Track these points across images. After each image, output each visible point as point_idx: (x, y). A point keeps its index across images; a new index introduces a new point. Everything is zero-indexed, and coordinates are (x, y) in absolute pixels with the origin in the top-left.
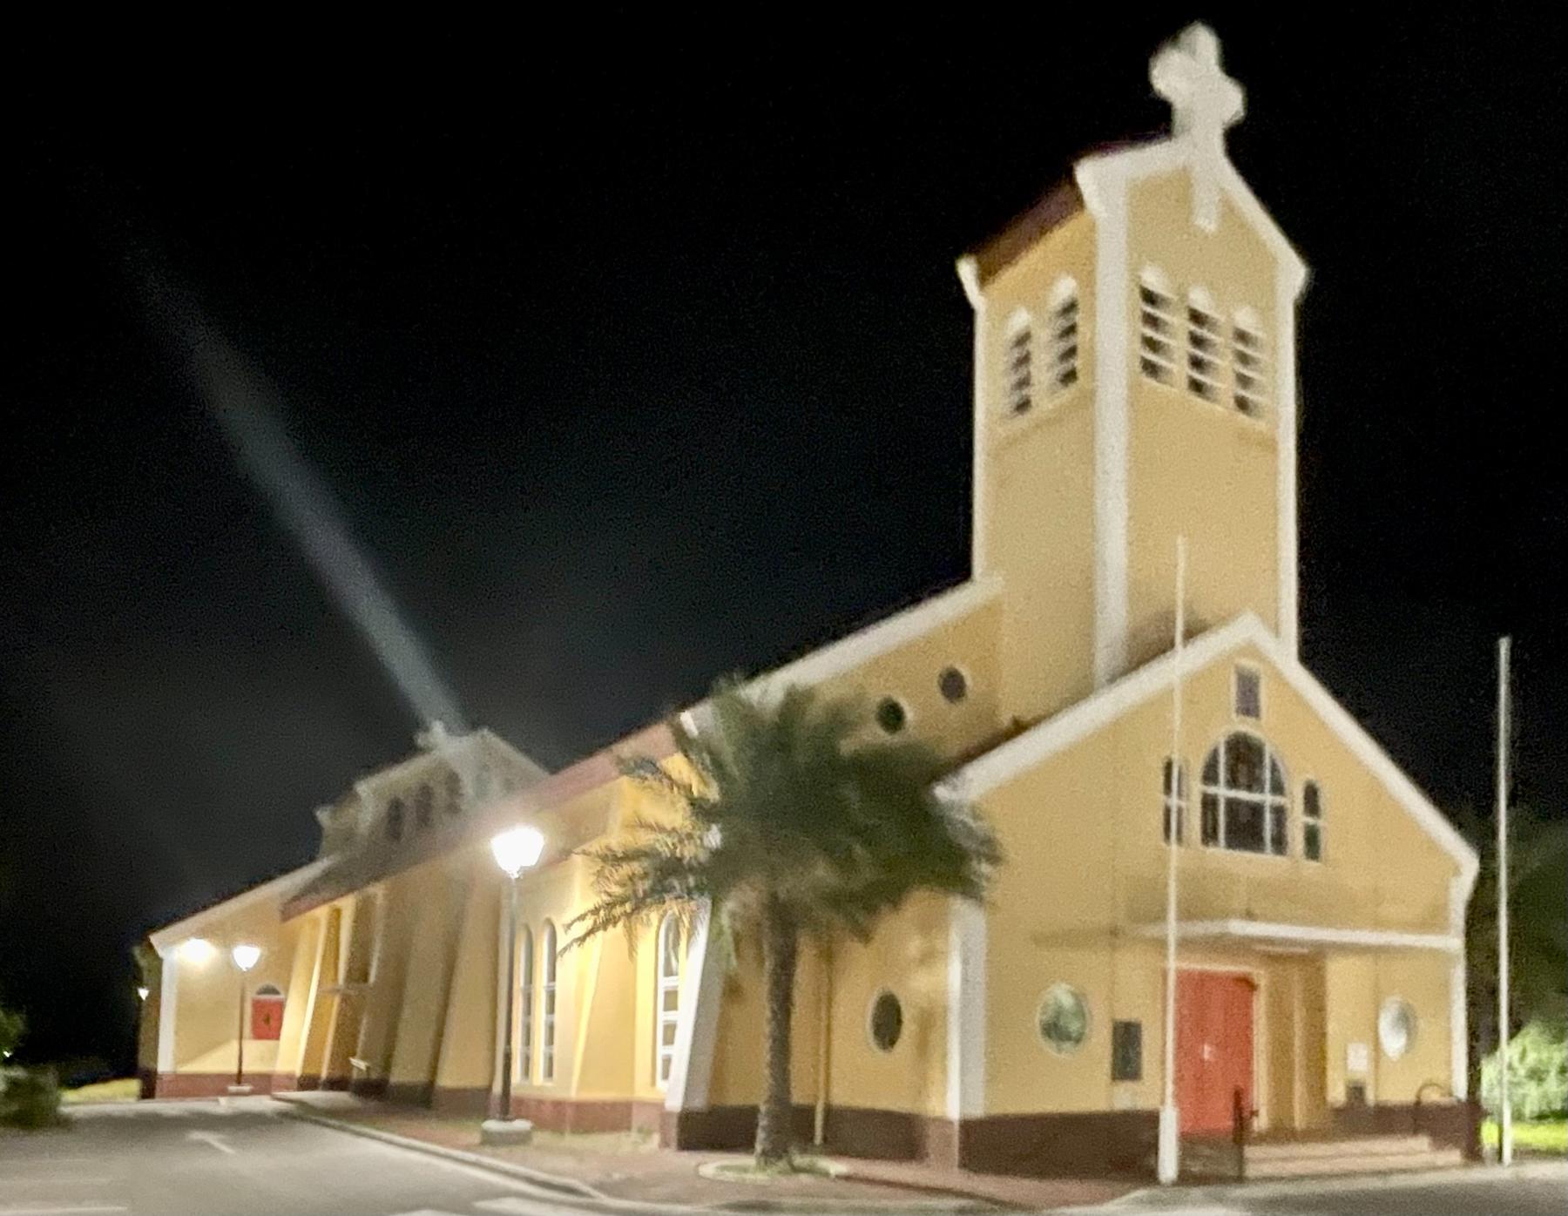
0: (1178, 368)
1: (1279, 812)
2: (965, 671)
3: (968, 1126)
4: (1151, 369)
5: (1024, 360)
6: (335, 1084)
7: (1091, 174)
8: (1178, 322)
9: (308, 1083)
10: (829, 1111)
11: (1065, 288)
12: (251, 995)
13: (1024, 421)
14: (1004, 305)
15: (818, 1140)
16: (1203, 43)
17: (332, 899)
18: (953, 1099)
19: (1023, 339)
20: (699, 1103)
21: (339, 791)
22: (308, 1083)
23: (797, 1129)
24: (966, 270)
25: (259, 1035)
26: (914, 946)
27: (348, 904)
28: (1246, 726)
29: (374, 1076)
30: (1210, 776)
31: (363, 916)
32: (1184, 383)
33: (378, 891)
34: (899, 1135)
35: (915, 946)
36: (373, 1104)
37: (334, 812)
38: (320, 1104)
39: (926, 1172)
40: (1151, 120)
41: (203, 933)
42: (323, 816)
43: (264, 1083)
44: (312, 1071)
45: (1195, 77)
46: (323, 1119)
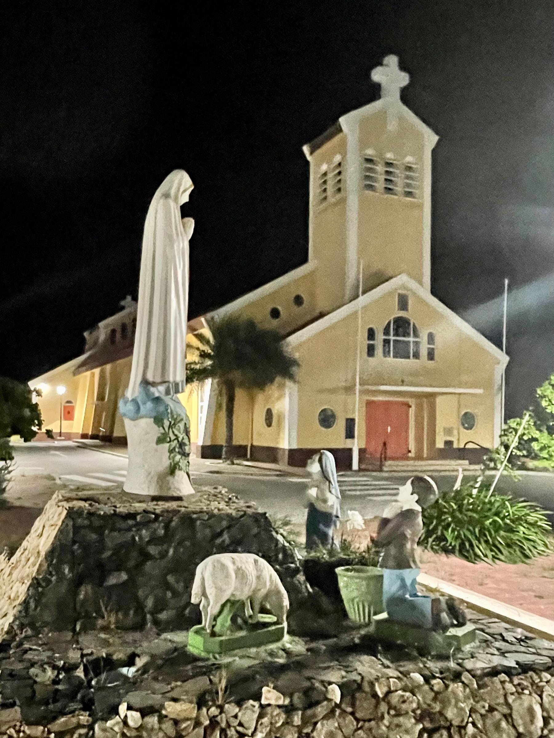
0: (380, 185)
1: (417, 344)
2: (280, 308)
3: (291, 451)
4: (370, 187)
5: (325, 182)
6: (93, 437)
7: (342, 120)
8: (380, 168)
9: (84, 436)
10: (252, 446)
11: (338, 158)
12: (63, 404)
13: (324, 204)
14: (319, 162)
15: (249, 456)
16: (392, 60)
17: (91, 369)
18: (286, 442)
19: (325, 174)
20: (208, 443)
21: (93, 325)
22: (84, 436)
23: (238, 452)
24: (306, 149)
25: (66, 419)
26: (276, 394)
27: (97, 371)
28: (402, 314)
29: (108, 434)
30: (386, 332)
31: (102, 377)
32: (383, 191)
33: (108, 367)
34: (271, 454)
35: (276, 394)
36: (107, 444)
37: (91, 333)
38: (89, 443)
39: (278, 466)
40: (374, 92)
41: (45, 381)
42: (86, 334)
43: (69, 436)
44: (86, 432)
45: (390, 75)
46: (94, 449)
